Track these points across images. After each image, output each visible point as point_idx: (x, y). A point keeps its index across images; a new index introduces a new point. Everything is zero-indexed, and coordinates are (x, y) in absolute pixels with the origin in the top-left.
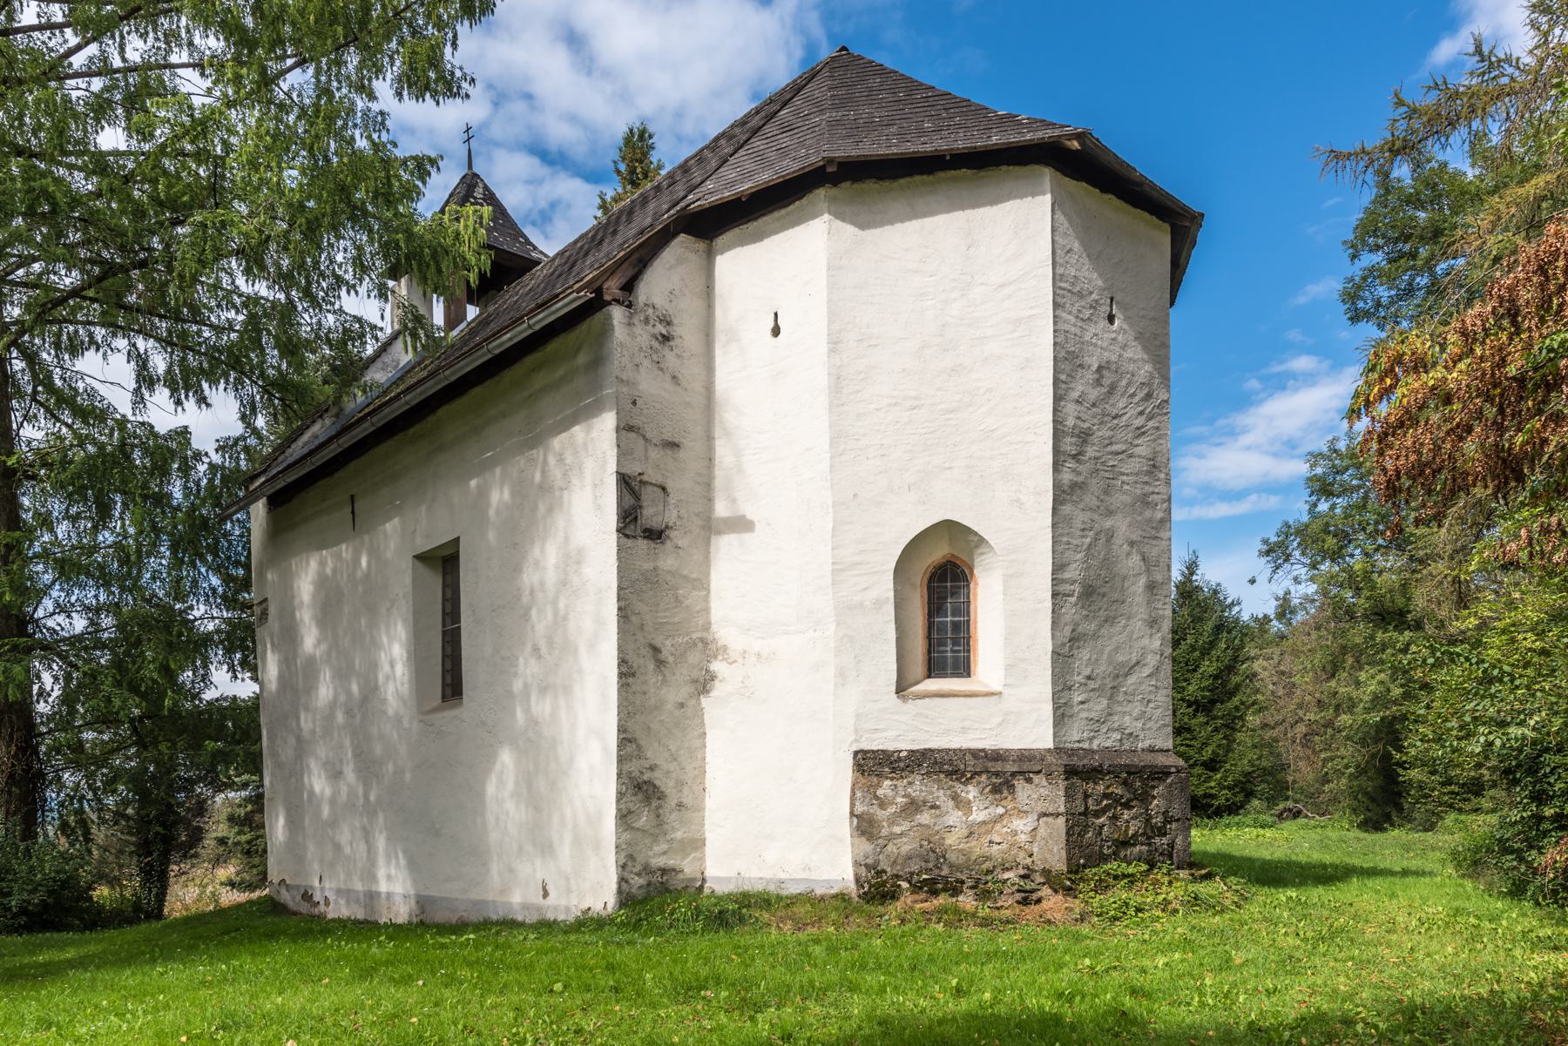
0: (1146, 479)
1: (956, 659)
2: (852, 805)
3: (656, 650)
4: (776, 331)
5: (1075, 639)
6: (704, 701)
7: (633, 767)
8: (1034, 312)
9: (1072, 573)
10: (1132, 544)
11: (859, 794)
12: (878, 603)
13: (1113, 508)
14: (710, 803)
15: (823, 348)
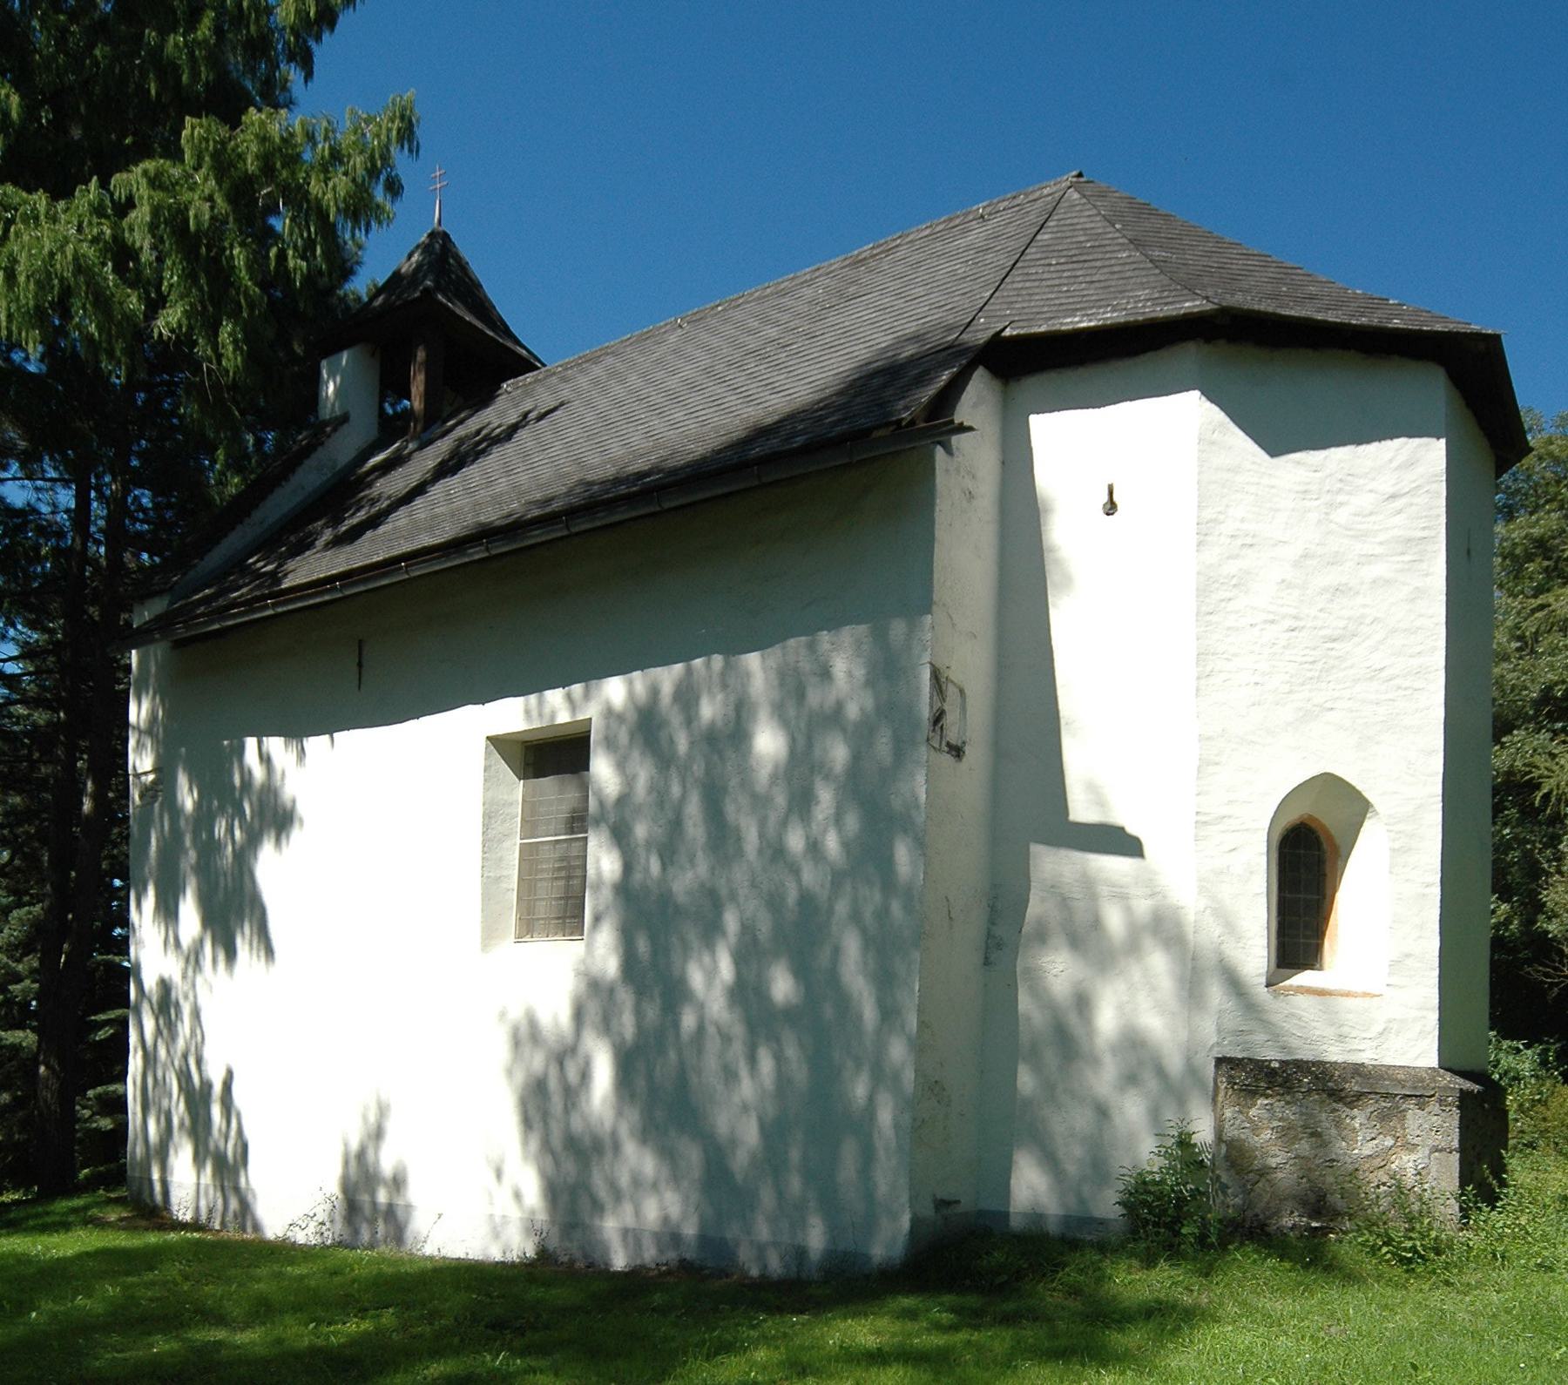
4: (1111, 508)
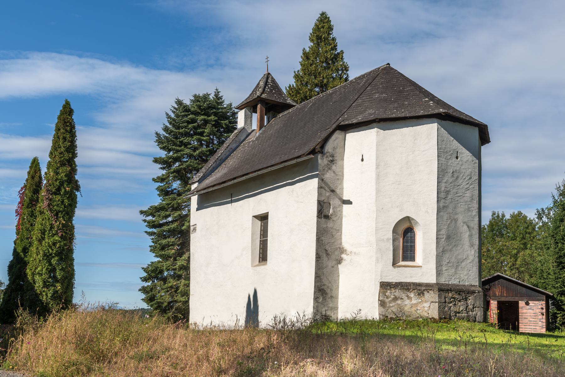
0: (469, 203)
1: (411, 256)
2: (379, 297)
3: (326, 250)
4: (362, 160)
5: (443, 251)
6: (339, 266)
8: (432, 158)
9: (443, 232)
10: (464, 223)
11: (381, 294)
12: (388, 240)
13: (458, 212)
14: (341, 296)
15: (375, 167)
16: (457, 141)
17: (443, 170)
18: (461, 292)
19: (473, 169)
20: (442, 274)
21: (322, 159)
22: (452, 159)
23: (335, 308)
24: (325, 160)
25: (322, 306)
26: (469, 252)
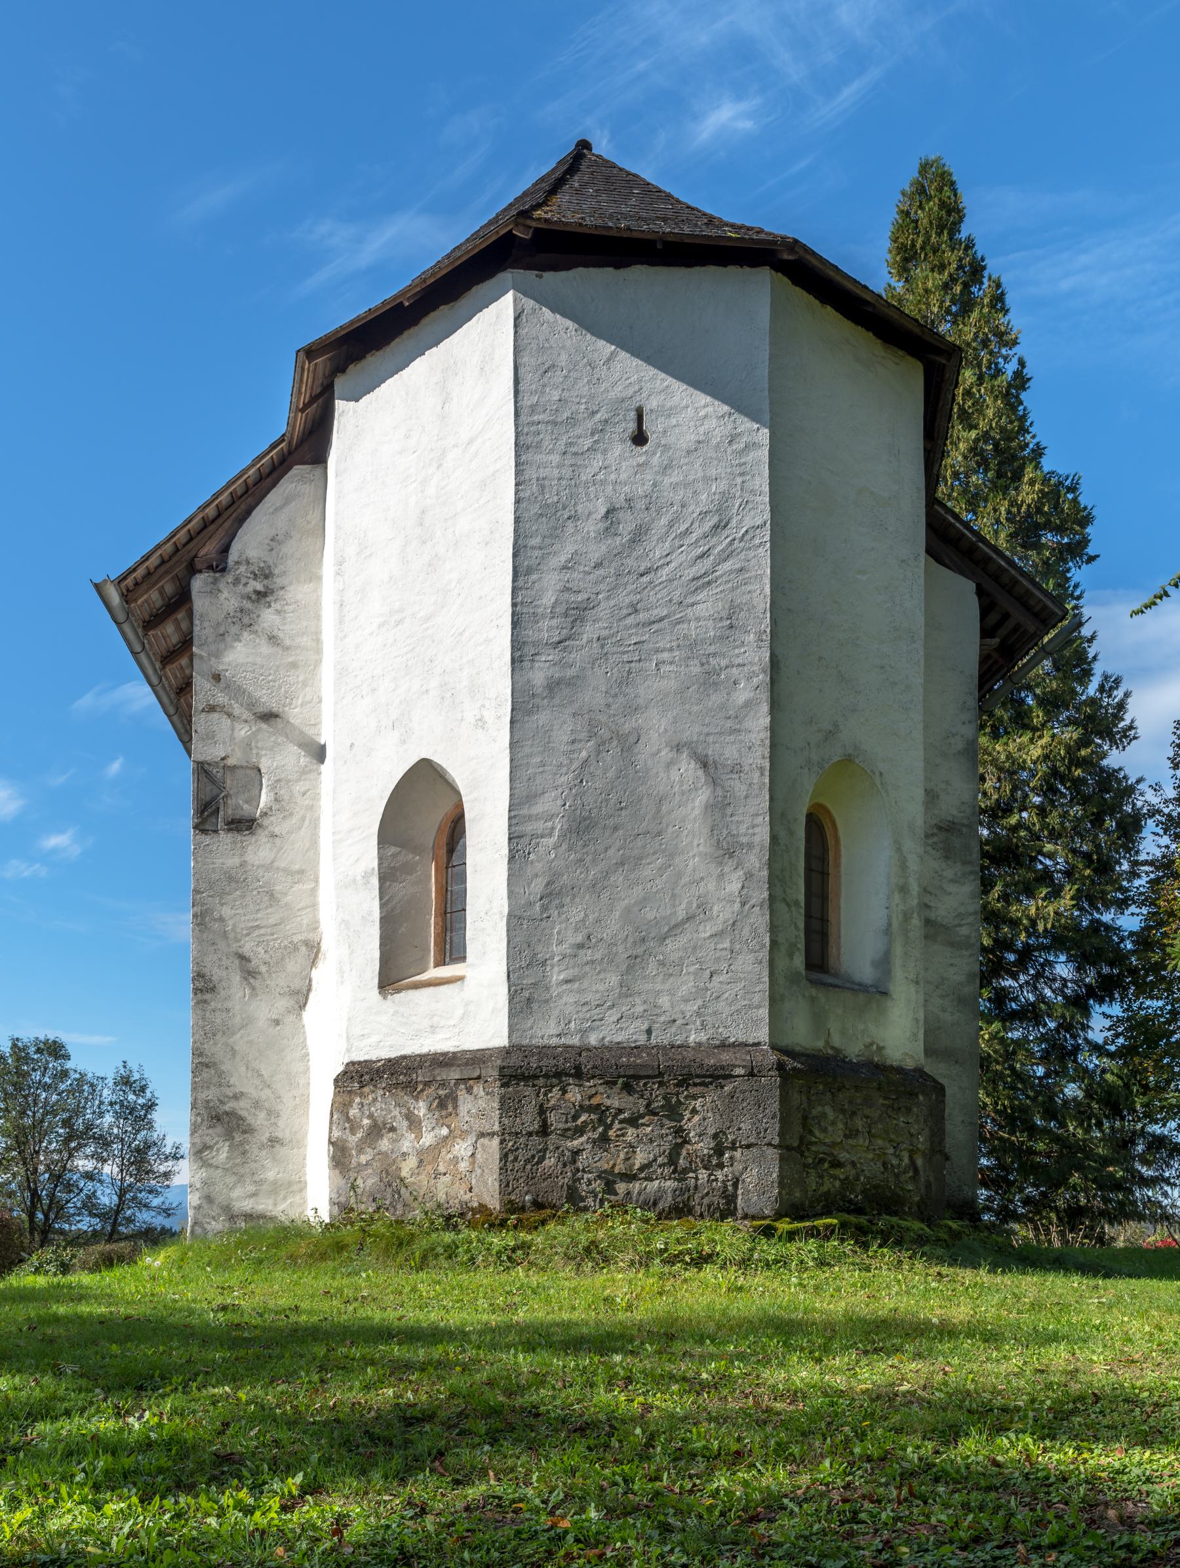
0: (712, 649)
3: (243, 958)
5: (552, 895)
7: (211, 1094)
9: (548, 803)
10: (678, 748)
13: (640, 701)
16: (635, 353)
17: (548, 511)
18: (637, 1077)
19: (739, 480)
20: (547, 1001)
21: (214, 592)
22: (604, 452)
23: (290, 1184)
24: (225, 594)
25: (230, 1180)
26: (712, 886)
